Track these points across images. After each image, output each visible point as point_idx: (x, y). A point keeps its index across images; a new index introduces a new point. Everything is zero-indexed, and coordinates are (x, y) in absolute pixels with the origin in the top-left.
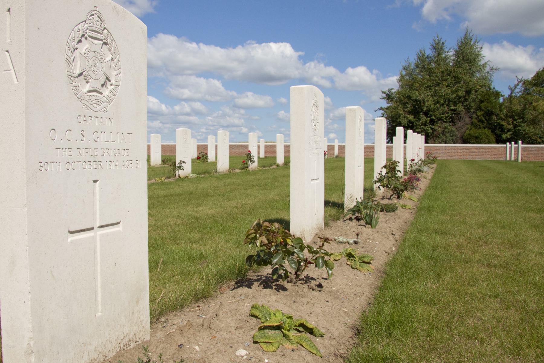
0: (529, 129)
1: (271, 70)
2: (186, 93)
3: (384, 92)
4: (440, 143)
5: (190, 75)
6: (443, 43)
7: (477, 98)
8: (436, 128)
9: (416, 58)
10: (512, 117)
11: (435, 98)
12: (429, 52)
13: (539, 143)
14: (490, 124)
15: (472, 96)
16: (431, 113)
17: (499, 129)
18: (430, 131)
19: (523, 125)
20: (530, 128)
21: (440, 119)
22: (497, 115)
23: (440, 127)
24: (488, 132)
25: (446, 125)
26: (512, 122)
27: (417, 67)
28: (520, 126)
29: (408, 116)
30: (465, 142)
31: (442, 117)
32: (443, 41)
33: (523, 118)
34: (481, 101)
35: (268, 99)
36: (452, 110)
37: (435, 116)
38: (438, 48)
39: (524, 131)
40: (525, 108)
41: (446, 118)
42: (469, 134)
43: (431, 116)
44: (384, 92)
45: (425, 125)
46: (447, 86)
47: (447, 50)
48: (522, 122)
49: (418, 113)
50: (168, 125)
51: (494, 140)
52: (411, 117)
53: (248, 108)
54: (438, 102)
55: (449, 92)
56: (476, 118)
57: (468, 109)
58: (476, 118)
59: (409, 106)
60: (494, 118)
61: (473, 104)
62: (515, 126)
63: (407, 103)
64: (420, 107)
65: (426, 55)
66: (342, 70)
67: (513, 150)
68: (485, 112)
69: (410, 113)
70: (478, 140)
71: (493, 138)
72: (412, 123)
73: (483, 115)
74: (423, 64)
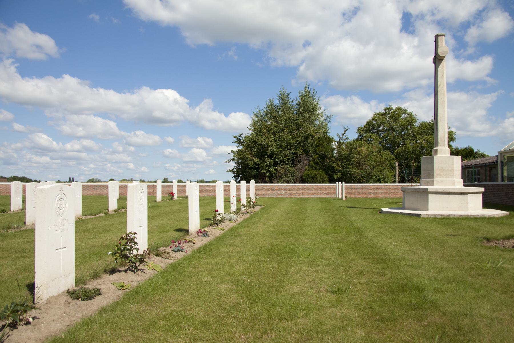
0: (354, 171)
1: (158, 114)
2: (80, 131)
3: (235, 137)
4: (283, 182)
5: (90, 115)
6: (288, 95)
7: (314, 143)
8: (279, 169)
9: (266, 106)
10: (341, 160)
11: (279, 142)
12: (276, 102)
13: (364, 182)
14: (324, 166)
15: (310, 141)
16: (275, 156)
17: (331, 170)
18: (274, 172)
19: (350, 166)
20: (355, 169)
21: (282, 161)
22: (329, 158)
23: (282, 168)
24: (322, 172)
25: (287, 166)
26: (341, 164)
27: (267, 114)
28: (347, 168)
29: (254, 159)
30: (303, 181)
31: (284, 160)
32: (288, 92)
33: (350, 161)
34: (317, 146)
35: (157, 138)
36: (293, 153)
37: (278, 159)
38: (284, 98)
39: (351, 172)
40: (351, 153)
41: (287, 161)
42: (307, 175)
43: (275, 158)
44: (235, 137)
45: (270, 166)
46: (289, 133)
47: (291, 100)
48: (349, 164)
49: (264, 156)
50: (57, 161)
51: (327, 180)
52: (257, 160)
53: (139, 146)
54: (281, 146)
55: (290, 137)
56: (313, 161)
57: (306, 152)
58: (313, 161)
59: (255, 150)
60: (327, 159)
61: (310, 149)
62: (344, 168)
63: (254, 147)
64: (265, 151)
65: (275, 104)
66: (227, 115)
67: (340, 189)
68: (320, 155)
69: (256, 156)
70: (313, 180)
71: (326, 178)
72: (258, 165)
73: (318, 158)
74: (272, 112)
